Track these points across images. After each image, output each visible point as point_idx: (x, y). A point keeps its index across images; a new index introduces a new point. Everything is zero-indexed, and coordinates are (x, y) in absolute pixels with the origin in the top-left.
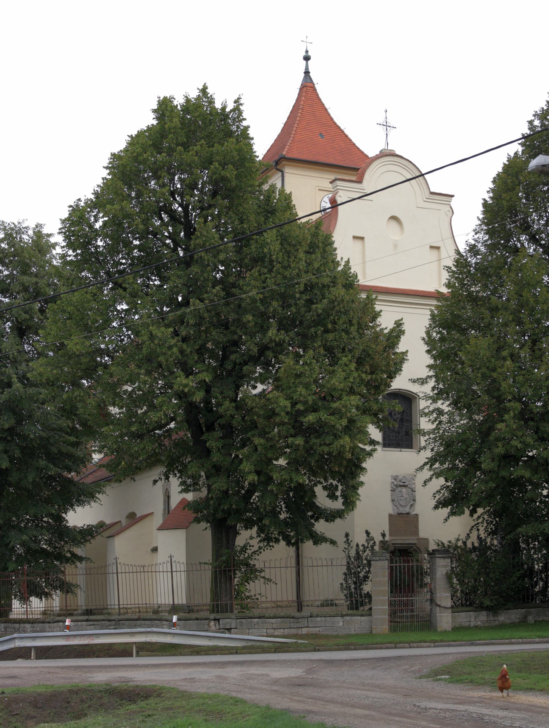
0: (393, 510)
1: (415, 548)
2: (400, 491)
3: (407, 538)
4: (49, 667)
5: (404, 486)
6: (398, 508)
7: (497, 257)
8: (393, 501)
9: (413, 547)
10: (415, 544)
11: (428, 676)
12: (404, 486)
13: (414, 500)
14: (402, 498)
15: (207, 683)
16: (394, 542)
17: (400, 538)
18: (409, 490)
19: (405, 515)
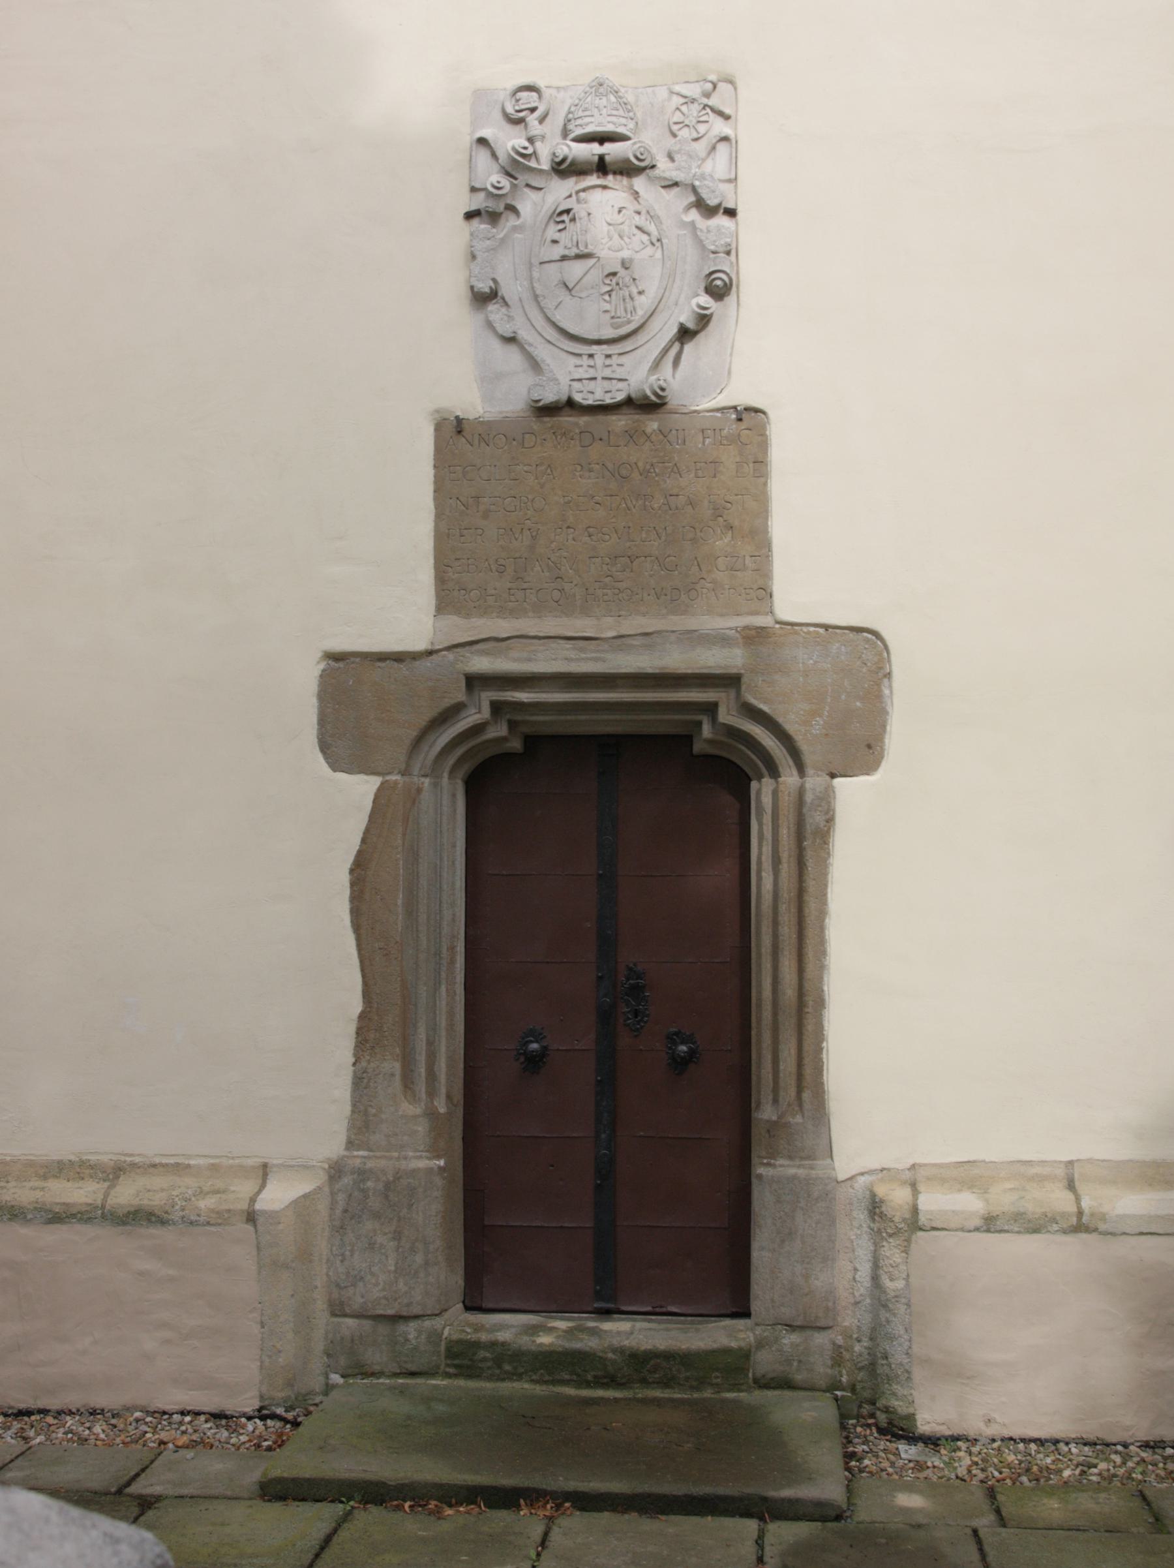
0: (490, 379)
1: (727, 716)
2: (563, 215)
3: (633, 624)
4: (775, 923)
5: (602, 167)
6: (535, 365)
7: (1011, 1479)
8: (484, 298)
9: (711, 709)
10: (731, 681)
11: (1071, 1232)
12: (602, 167)
13: (719, 290)
14: (576, 269)
15: (42, 1193)
16: (481, 664)
17: (552, 625)
18: (672, 205)
19: (620, 422)
